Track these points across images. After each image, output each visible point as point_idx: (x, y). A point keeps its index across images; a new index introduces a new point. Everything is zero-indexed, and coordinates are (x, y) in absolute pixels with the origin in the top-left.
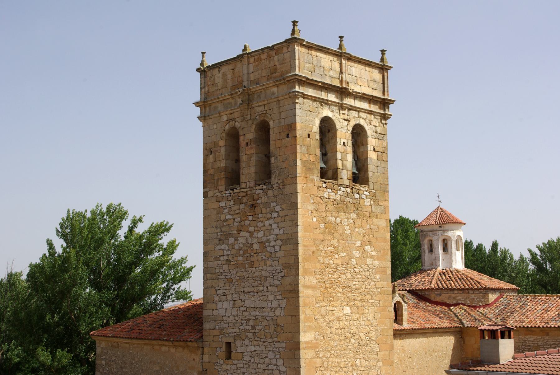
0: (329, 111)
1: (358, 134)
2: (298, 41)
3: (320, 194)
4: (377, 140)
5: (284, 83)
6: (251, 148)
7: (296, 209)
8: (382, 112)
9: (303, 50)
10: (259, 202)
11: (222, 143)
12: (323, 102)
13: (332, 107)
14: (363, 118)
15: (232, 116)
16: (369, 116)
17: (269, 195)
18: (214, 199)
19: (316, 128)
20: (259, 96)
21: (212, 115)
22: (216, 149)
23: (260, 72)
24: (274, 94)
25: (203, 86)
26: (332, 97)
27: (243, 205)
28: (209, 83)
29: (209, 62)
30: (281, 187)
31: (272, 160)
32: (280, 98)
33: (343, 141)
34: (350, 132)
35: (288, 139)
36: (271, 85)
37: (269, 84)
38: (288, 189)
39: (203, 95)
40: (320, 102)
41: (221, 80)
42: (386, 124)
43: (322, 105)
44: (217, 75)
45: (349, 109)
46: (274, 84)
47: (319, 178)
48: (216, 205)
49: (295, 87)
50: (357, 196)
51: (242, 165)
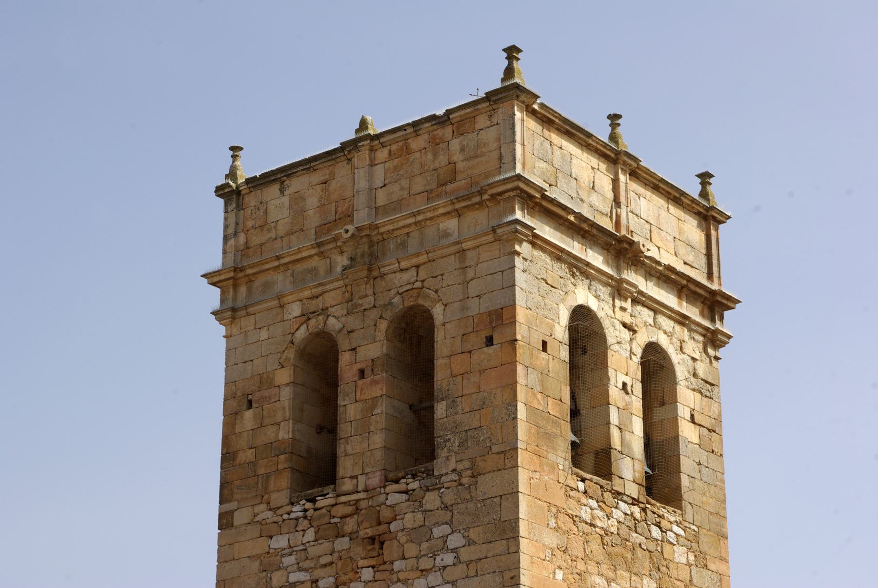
0: (590, 296)
1: (655, 366)
2: (523, 97)
3: (572, 507)
4: (698, 395)
5: (480, 203)
6: (375, 382)
7: (515, 537)
8: (706, 323)
9: (532, 124)
10: (393, 527)
11: (284, 376)
12: (578, 269)
13: (596, 285)
14: (665, 333)
15: (319, 303)
16: (678, 328)
17: (428, 506)
18: (254, 531)
19: (561, 332)
20: (403, 245)
21: (258, 303)
22: (265, 393)
23: (405, 183)
24: (446, 235)
25: (231, 231)
26: (596, 259)
27: (346, 539)
28: (250, 223)
29: (250, 168)
30: (465, 480)
31: (440, 409)
32: (465, 246)
33: (622, 378)
34: (637, 359)
35: (490, 350)
36: (442, 211)
37: (435, 209)
38: (488, 485)
39: (231, 256)
40: (571, 266)
41: (286, 212)
42: (717, 358)
43: (573, 275)
44: (277, 202)
45: (635, 301)
46: (449, 208)
47: (568, 463)
48: (260, 546)
49: (513, 211)
50: (656, 532)
51: (344, 429)
